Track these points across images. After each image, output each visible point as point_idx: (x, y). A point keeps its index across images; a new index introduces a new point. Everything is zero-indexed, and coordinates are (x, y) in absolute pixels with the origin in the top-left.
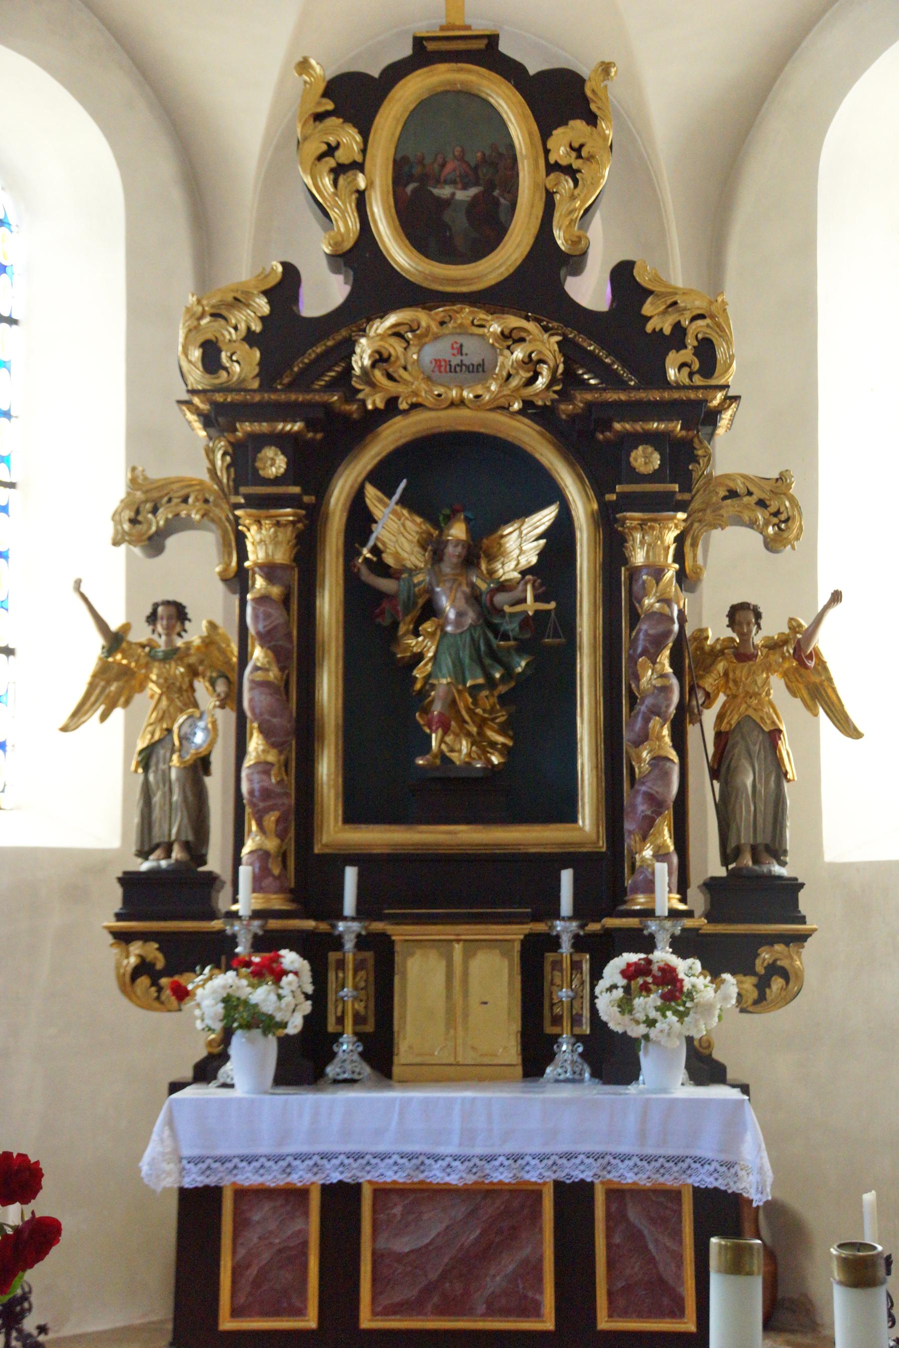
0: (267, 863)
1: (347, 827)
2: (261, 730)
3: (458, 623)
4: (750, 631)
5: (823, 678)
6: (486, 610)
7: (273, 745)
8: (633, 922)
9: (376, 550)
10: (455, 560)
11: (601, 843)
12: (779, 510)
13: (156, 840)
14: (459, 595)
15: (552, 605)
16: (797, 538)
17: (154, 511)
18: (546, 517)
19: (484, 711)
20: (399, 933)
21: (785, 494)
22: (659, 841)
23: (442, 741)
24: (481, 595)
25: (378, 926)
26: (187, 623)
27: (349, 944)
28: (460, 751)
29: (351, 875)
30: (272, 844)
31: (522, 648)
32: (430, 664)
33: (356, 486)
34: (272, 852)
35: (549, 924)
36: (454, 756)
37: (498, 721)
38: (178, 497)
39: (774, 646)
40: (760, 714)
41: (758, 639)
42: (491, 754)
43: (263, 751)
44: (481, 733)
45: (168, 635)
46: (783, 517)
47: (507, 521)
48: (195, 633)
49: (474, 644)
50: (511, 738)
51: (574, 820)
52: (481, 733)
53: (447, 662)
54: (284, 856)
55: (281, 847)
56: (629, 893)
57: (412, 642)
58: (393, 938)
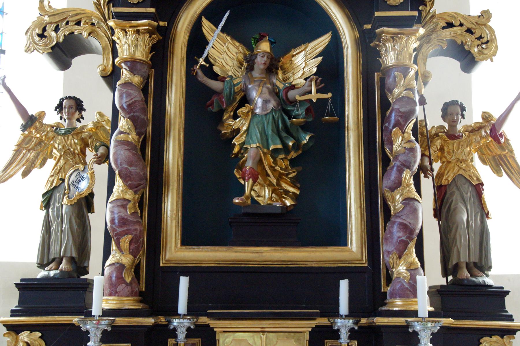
0: (122, 273)
1: (184, 247)
2: (121, 177)
3: (264, 108)
4: (458, 119)
5: (507, 151)
6: (284, 104)
7: (130, 187)
8: (400, 321)
9: (207, 60)
10: (262, 67)
11: (364, 262)
12: (481, 36)
13: (52, 257)
14: (265, 90)
15: (330, 95)
16: (494, 54)
17: (57, 29)
18: (322, 42)
19: (281, 169)
20: (217, 325)
21: (485, 25)
22: (410, 260)
23: (252, 189)
24: (279, 92)
25: (204, 320)
26: (83, 112)
27: (181, 335)
28: (264, 197)
29: (184, 282)
30: (127, 260)
31: (305, 127)
32: (244, 136)
33: (196, 16)
34: (126, 265)
35: (332, 320)
36: (260, 200)
37: (290, 176)
38: (73, 21)
39: (476, 130)
40: (468, 173)
41: (460, 127)
42: (284, 198)
43: (122, 191)
44: (278, 184)
45: (69, 119)
46: (485, 40)
47: (296, 46)
48: (89, 120)
49: (275, 123)
50: (299, 189)
51: (346, 244)
52: (278, 184)
53: (256, 133)
54: (137, 269)
55: (134, 261)
56: (388, 297)
57: (231, 122)
58: (215, 330)
